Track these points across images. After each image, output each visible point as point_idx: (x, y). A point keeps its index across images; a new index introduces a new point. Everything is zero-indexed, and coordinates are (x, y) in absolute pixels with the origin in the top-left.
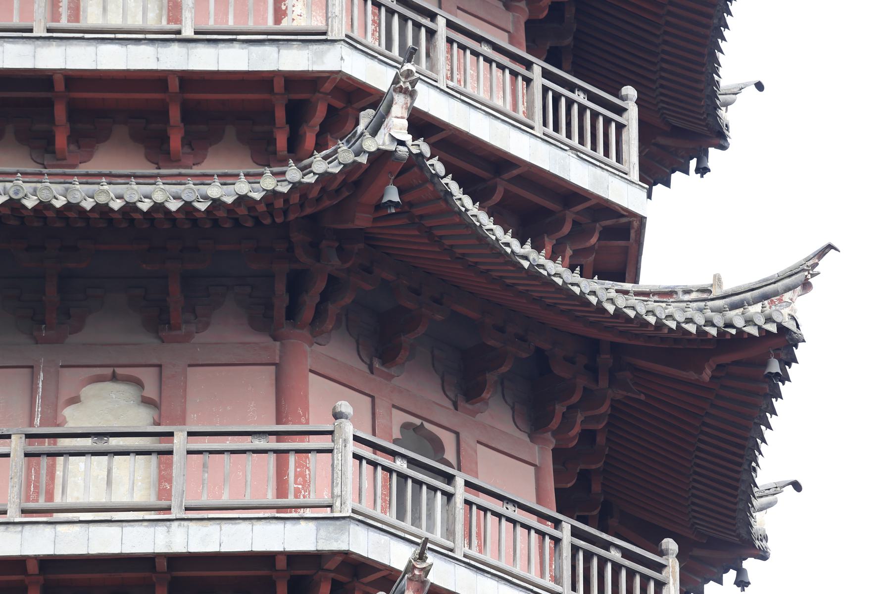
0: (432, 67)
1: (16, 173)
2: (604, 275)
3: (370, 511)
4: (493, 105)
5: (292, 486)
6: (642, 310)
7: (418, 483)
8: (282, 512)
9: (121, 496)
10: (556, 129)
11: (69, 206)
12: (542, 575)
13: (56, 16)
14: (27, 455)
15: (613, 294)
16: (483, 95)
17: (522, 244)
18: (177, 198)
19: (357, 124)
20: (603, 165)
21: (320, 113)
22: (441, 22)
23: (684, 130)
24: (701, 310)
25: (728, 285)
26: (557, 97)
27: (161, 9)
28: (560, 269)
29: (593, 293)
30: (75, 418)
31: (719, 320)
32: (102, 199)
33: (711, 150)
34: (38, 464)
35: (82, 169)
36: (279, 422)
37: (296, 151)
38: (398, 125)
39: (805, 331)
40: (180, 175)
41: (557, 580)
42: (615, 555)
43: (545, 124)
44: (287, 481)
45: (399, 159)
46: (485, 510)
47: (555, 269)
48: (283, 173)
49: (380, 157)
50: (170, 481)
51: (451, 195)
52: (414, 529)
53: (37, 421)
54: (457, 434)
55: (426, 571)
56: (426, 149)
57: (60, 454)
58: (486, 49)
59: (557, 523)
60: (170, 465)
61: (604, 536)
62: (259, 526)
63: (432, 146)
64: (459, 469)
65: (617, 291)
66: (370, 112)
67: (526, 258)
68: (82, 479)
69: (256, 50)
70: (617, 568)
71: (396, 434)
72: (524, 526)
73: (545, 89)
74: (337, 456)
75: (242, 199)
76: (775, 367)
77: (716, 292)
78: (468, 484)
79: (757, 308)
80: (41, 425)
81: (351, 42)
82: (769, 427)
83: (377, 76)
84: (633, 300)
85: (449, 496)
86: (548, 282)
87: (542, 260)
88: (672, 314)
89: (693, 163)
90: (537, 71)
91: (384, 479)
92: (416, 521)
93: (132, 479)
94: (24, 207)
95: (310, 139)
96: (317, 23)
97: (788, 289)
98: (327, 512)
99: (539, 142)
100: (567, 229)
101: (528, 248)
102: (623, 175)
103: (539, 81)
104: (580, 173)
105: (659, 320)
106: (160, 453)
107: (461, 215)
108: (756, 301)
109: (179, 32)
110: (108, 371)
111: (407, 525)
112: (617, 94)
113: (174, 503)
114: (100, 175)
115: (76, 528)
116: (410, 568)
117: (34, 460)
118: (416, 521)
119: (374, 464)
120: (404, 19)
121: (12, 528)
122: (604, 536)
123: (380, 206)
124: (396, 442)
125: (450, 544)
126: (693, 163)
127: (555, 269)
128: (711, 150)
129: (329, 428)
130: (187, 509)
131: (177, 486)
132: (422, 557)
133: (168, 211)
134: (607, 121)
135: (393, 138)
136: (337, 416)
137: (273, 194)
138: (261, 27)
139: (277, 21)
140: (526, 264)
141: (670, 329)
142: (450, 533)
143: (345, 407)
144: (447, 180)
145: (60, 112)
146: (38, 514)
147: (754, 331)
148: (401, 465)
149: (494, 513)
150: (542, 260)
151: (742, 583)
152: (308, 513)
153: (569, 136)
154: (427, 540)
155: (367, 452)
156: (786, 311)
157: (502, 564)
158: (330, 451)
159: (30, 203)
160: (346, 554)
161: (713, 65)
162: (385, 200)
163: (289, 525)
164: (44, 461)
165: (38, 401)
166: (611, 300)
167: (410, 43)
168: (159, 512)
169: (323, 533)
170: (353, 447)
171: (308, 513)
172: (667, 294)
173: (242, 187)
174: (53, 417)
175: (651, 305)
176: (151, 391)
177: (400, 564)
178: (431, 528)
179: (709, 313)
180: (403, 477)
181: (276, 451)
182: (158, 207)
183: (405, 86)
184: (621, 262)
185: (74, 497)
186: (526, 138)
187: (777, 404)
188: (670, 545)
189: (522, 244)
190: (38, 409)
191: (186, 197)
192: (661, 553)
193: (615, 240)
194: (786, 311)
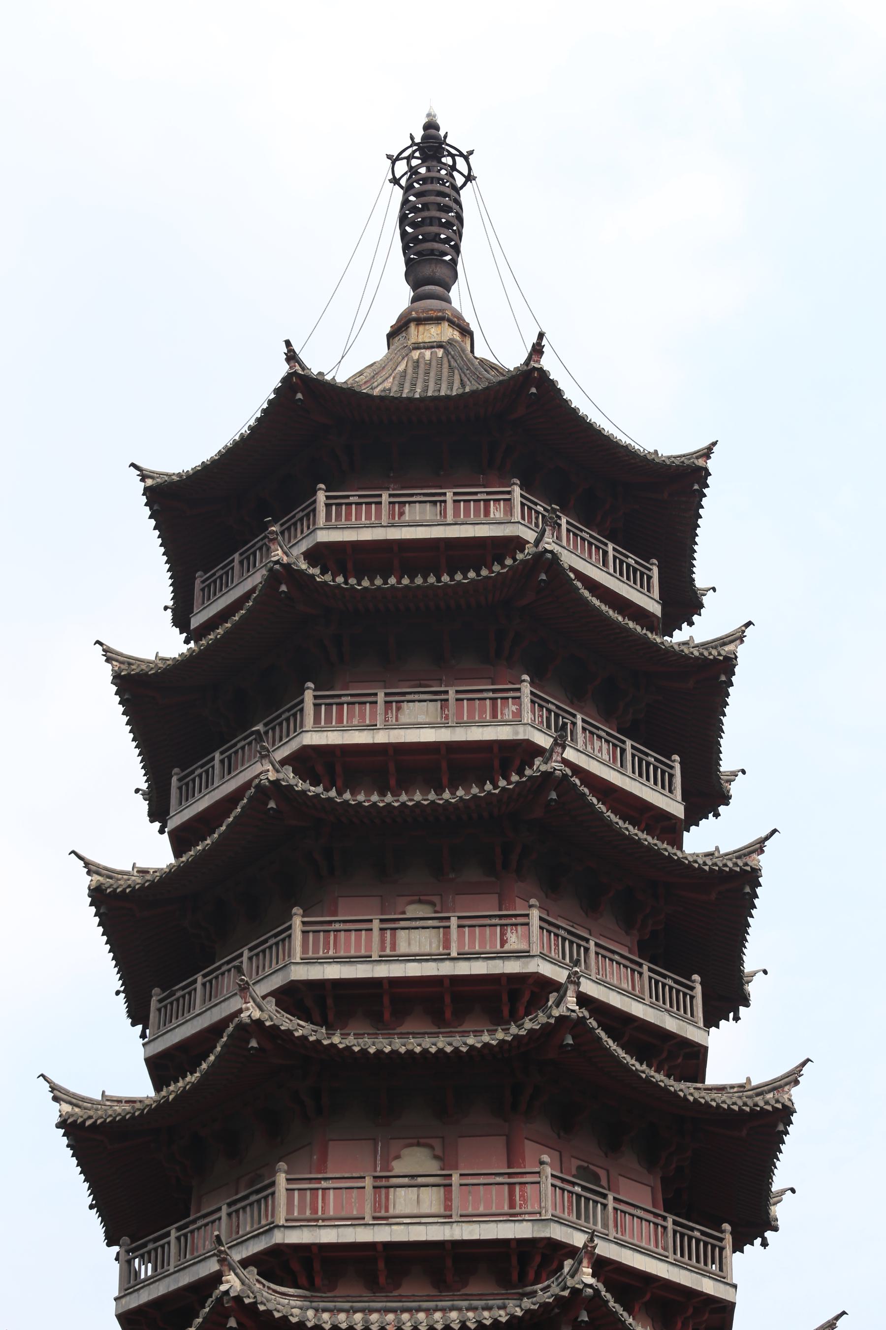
0: (587, 967)
1: (364, 1034)
2: (687, 1080)
3: (561, 1215)
4: (617, 986)
5: (518, 1202)
6: (708, 1099)
7: (587, 1199)
8: (512, 1217)
9: (425, 1209)
10: (657, 999)
11: (392, 1051)
12: (657, 1246)
13: (383, 948)
14: (374, 1187)
15: (692, 1090)
16: (615, 982)
17: (641, 1064)
18: (450, 1044)
19: (548, 1001)
20: (683, 1019)
21: (526, 997)
22: (592, 943)
23: (727, 997)
24: (740, 1097)
25: (754, 1083)
26: (657, 982)
27: (439, 942)
28: (663, 1078)
29: (681, 1090)
30: (399, 1167)
31: (750, 1103)
32: (410, 1047)
33: (741, 1008)
34: (380, 1192)
35: (398, 1031)
36: (509, 1167)
37: (515, 1017)
38: (571, 1001)
39: (796, 1106)
40: (451, 1032)
41: (665, 1249)
42: (697, 1234)
43: (651, 997)
44: (515, 1200)
45: (572, 1020)
46: (625, 1213)
47: (659, 1078)
48: (508, 1029)
49: (561, 1019)
50: (451, 1200)
51: (601, 1039)
52: (586, 1224)
53: (378, 1169)
54: (608, 1171)
55: (594, 1247)
56: (587, 1014)
57: (392, 1187)
58: (617, 957)
59: (665, 1219)
60: (451, 1191)
61: (691, 1224)
62: (500, 1225)
63: (590, 1011)
64: (609, 1190)
65: (695, 1088)
66: (555, 994)
67: (643, 1072)
68: (403, 1200)
69: (491, 963)
70: (698, 1241)
71: (574, 1172)
72: (646, 1220)
73: (650, 978)
74: (543, 1186)
75: (486, 1045)
76: (781, 1128)
77: (748, 1087)
78: (615, 1199)
79: (770, 1095)
80: (381, 1171)
81: (543, 956)
82: (778, 1160)
83: (560, 975)
84: (703, 1094)
85: (605, 1206)
86: (656, 1085)
87: (652, 1073)
88: (724, 1100)
89: (731, 1015)
90: (645, 968)
91: (568, 1197)
92: (587, 1219)
93: (430, 1200)
94: (369, 1053)
95: (522, 1011)
96: (523, 946)
97: (786, 1084)
98: (538, 1217)
99: (648, 1008)
100: (664, 1055)
101: (644, 1067)
102: (694, 1024)
103: (646, 974)
104: (671, 1024)
105: (718, 1104)
106: (445, 1186)
107: (607, 1051)
108: (770, 1091)
109: (449, 954)
110: (415, 1141)
111: (582, 1222)
112: (670, 759)
113: (454, 1213)
114: (409, 1033)
115: (402, 1227)
116: (585, 1246)
117: (378, 1190)
118: (587, 1219)
119: (563, 1190)
120: (571, 943)
121: (368, 1227)
122: (691, 1224)
123: (562, 1046)
124: (574, 1176)
125: (606, 1232)
126: (731, 1015)
127: (659, 1078)
128: (741, 1008)
129: (537, 1170)
130: (461, 1216)
131: (456, 1202)
132: (592, 1240)
133: (445, 1053)
134: (685, 995)
135: (568, 1009)
136: (542, 1163)
137: (502, 1042)
138: (494, 950)
139: (502, 946)
140: (644, 1076)
141: (724, 1109)
142: (605, 1225)
143: (546, 1158)
144: (599, 1031)
145: (386, 1000)
146: (382, 1219)
147: (769, 1108)
148: (578, 1189)
149: (630, 1214)
150: (652, 1073)
151: (765, 1244)
152: (527, 1217)
153: (664, 1003)
154: (594, 1231)
155: (558, 1183)
156: (786, 1096)
157: (635, 1242)
158: (539, 1183)
159: (372, 1050)
160: (549, 1239)
161: (740, 962)
162: (579, 1319)
163: (517, 1224)
164: (383, 1191)
165: (379, 1158)
166: (691, 1094)
167: (575, 957)
168: (446, 1217)
169: (536, 1228)
170: (550, 1180)
171: (527, 1217)
172: (721, 1089)
173: (486, 1038)
174: (386, 1167)
175: (714, 1096)
176: (438, 1152)
177: (580, 1244)
178: (595, 1223)
179: (745, 1099)
180: (579, 1196)
181: (509, 1184)
182: (441, 1051)
183: (574, 979)
184: (697, 1072)
185: (399, 1211)
186: (641, 1005)
187: (782, 1147)
188: (727, 1227)
189: (641, 1064)
190: (379, 1162)
191: (455, 1044)
192: (722, 1232)
193: (692, 1060)
194: (786, 1096)
